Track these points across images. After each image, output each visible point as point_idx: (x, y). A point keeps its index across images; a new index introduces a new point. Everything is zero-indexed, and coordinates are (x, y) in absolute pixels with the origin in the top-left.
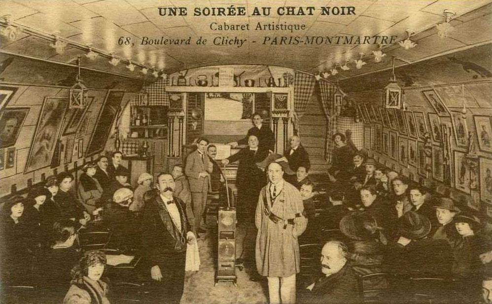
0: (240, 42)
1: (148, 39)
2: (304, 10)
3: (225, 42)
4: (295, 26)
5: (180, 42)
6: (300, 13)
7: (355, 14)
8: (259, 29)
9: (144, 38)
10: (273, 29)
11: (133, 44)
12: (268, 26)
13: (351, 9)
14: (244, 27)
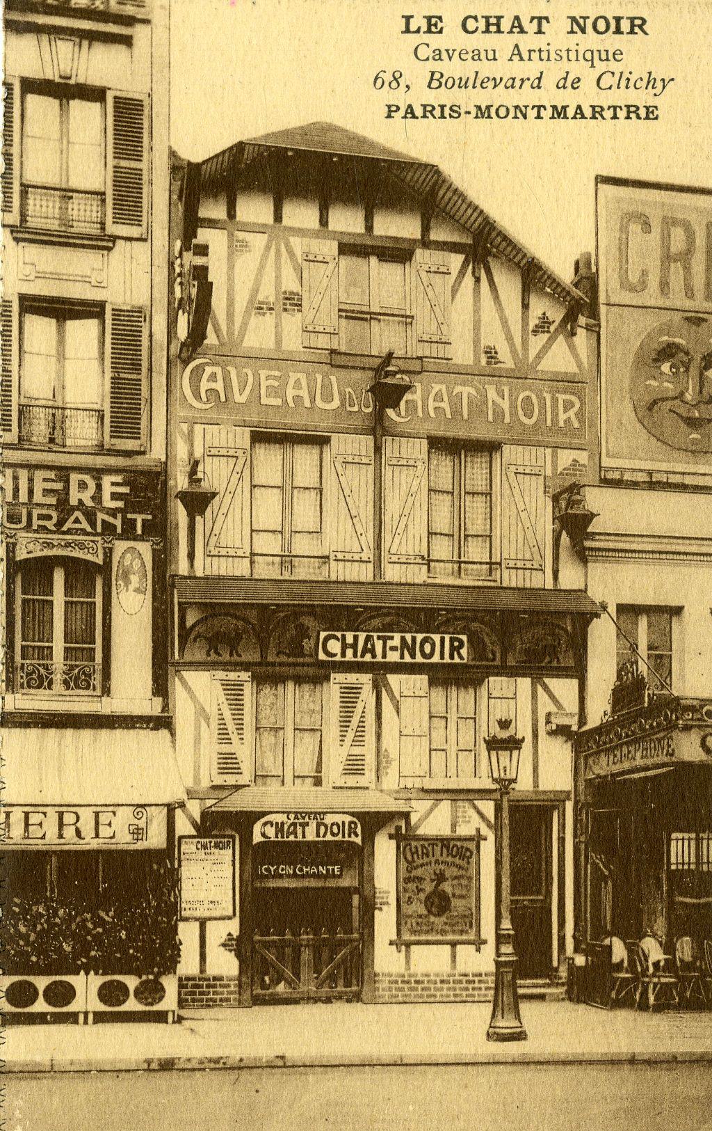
0: (659, 85)
1: (442, 76)
2: (525, 23)
3: (623, 83)
4: (599, 51)
5: (518, 83)
6: (514, 30)
7: (646, 34)
8: (516, 58)
9: (433, 74)
10: (549, 59)
11: (408, 87)
12: (537, 53)
13: (638, 22)
14: (467, 53)
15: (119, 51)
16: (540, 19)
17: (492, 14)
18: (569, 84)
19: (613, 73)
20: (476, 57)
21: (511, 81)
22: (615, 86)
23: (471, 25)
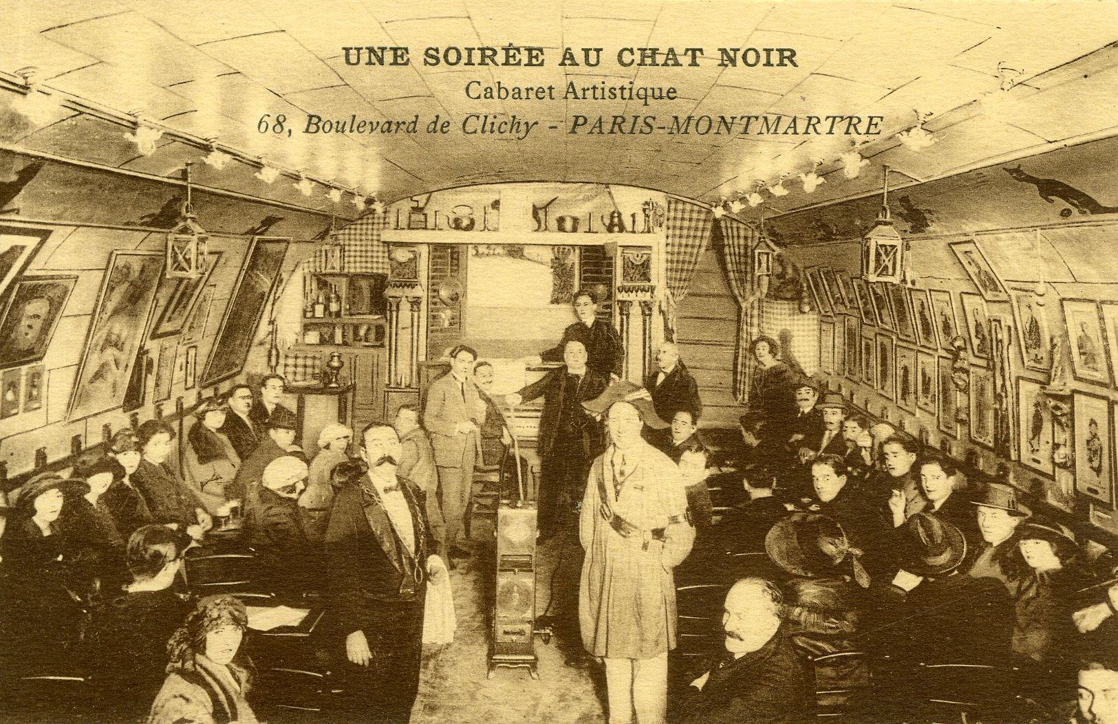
0: (523, 128)
5: (394, 127)
6: (669, 62)
7: (795, 65)
15: (20, 96)
16: (694, 50)
17: (593, 47)
18: (439, 127)
19: (478, 117)
20: (516, 96)
21: (387, 125)
22: (479, 131)
23: (627, 57)
